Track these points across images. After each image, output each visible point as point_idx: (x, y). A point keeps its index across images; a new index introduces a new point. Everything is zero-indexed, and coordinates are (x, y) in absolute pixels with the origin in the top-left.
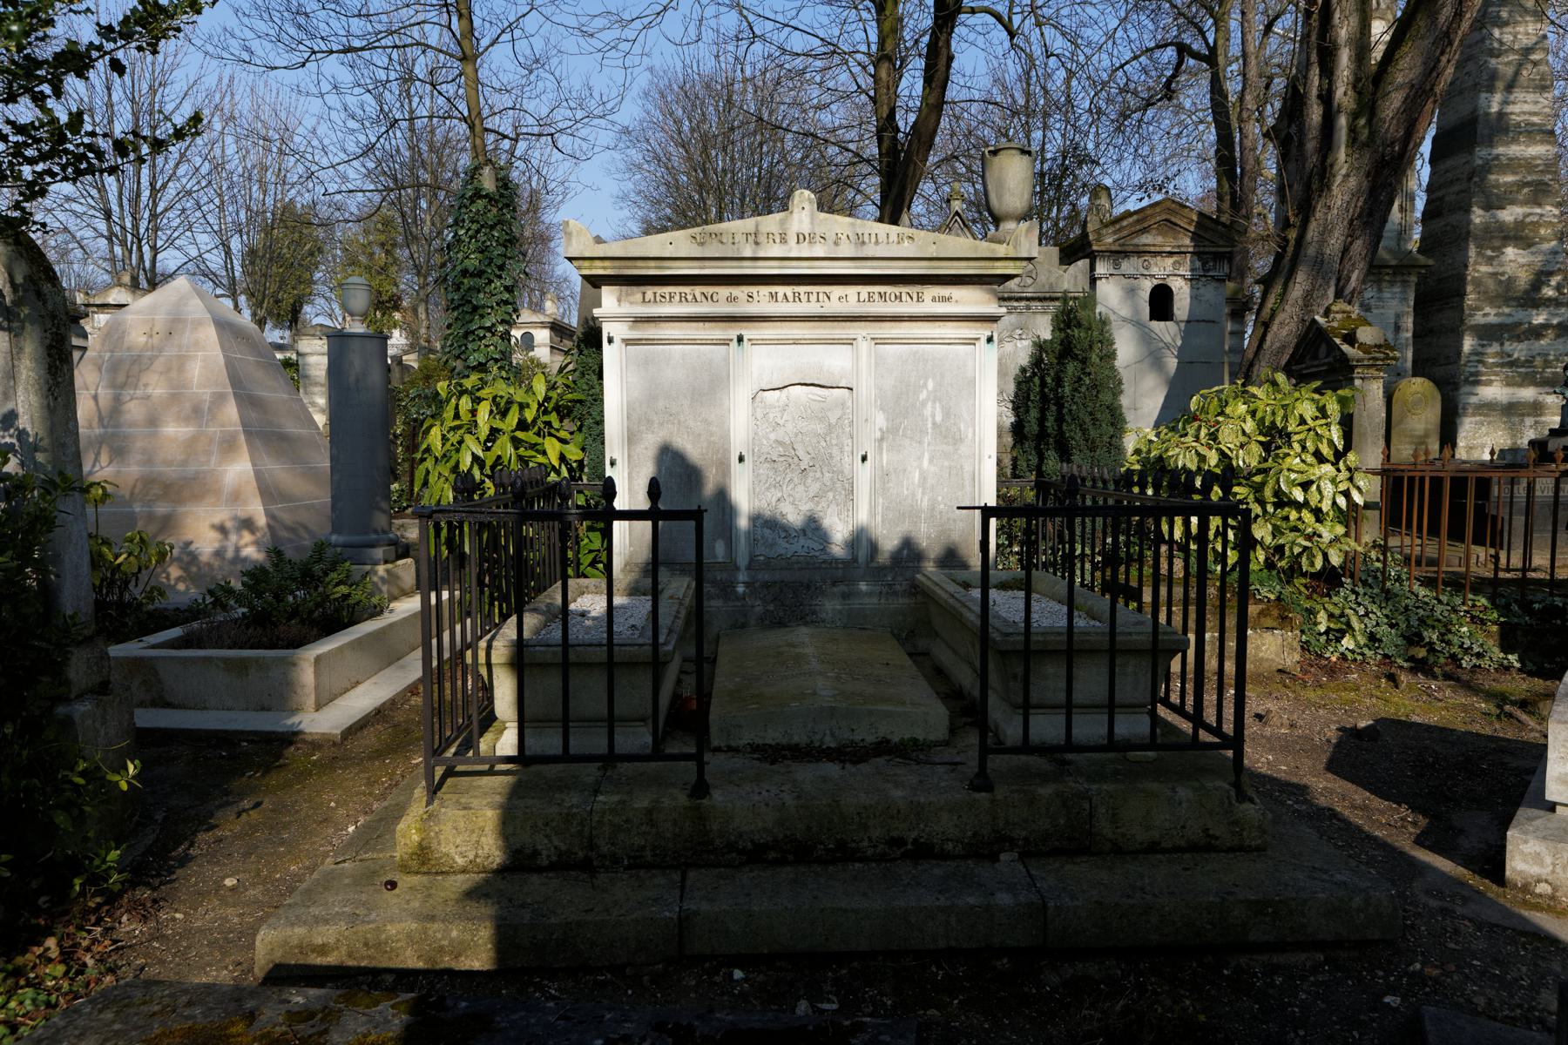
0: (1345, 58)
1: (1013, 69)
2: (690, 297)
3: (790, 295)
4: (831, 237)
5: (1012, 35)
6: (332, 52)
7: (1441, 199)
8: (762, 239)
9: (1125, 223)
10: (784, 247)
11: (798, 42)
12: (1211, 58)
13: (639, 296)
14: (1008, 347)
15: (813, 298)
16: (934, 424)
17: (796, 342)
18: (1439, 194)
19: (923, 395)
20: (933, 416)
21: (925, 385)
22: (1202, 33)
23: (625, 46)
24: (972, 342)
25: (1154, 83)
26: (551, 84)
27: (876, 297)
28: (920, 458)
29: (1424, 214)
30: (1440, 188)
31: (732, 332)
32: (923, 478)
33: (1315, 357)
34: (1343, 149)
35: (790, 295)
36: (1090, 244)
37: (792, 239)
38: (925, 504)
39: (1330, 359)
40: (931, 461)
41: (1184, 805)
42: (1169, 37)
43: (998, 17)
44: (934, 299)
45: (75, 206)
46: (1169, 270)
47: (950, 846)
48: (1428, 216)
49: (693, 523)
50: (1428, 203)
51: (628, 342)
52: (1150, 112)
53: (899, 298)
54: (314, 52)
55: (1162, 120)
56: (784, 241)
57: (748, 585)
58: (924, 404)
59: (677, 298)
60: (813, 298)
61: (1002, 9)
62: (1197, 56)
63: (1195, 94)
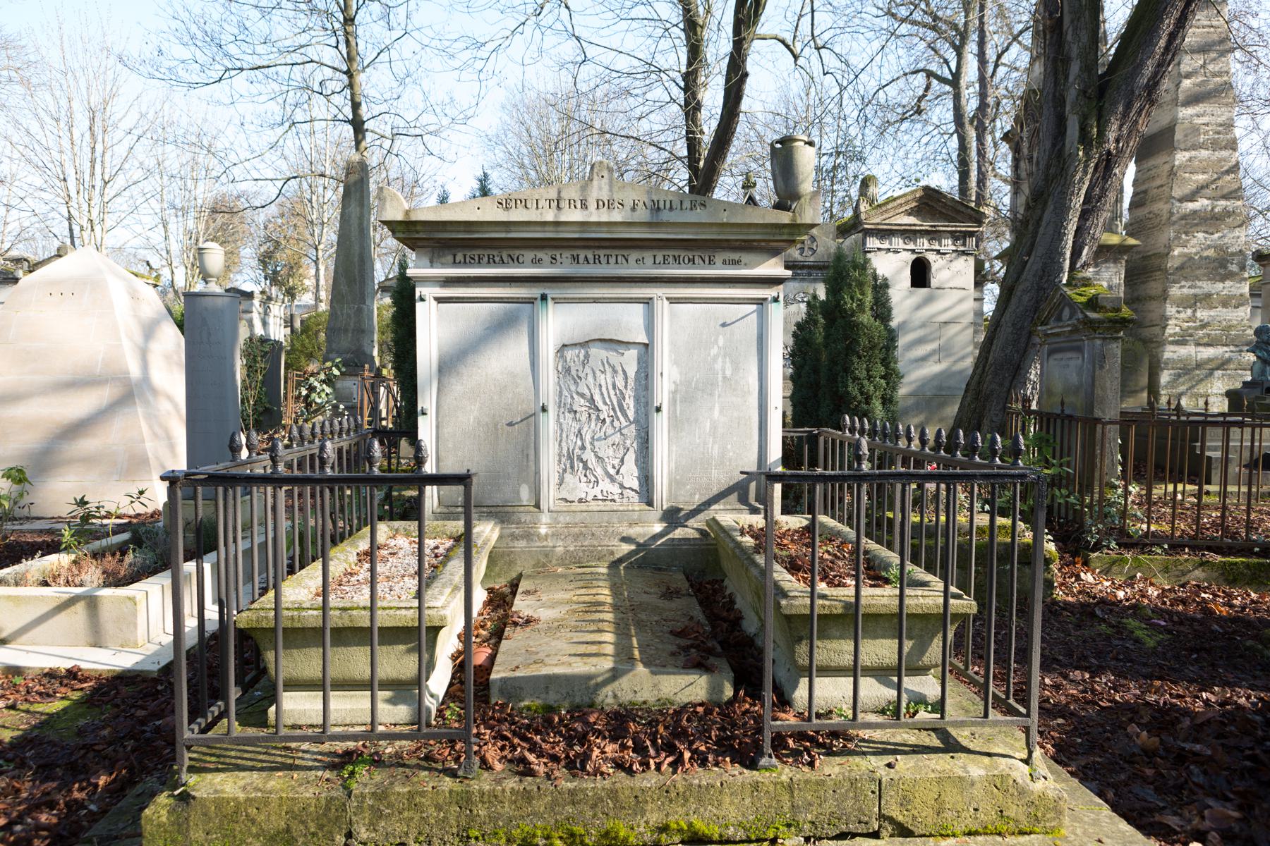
0: (1075, 68)
1: (797, 86)
2: (497, 259)
3: (590, 257)
4: (629, 204)
5: (796, 57)
6: (242, 69)
7: (1145, 192)
8: (564, 204)
9: (889, 206)
10: (585, 212)
11: (623, 63)
12: (955, 81)
13: (450, 258)
14: (793, 308)
15: (612, 260)
16: (724, 377)
17: (596, 301)
18: (1143, 188)
19: (714, 351)
20: (724, 370)
21: (716, 341)
22: (946, 62)
23: (479, 64)
24: (531, 301)
25: (907, 99)
26: (418, 96)
27: (671, 259)
28: (711, 409)
29: (1131, 204)
30: (1144, 182)
31: (535, 292)
32: (714, 428)
33: (1059, 319)
34: (349, 707)
35: (590, 257)
36: (861, 223)
37: (592, 205)
38: (716, 452)
39: (1074, 321)
40: (721, 412)
41: (978, 785)
42: (921, 66)
43: (783, 42)
44: (724, 262)
45: (43, 195)
46: (927, 246)
47: (731, 831)
48: (1133, 206)
49: (461, 488)
50: (1135, 194)
51: (440, 300)
52: (905, 125)
53: (692, 261)
54: (227, 70)
55: (911, 133)
56: (584, 206)
57: (550, 526)
58: (715, 360)
59: (486, 259)
60: (612, 260)
61: (789, 38)
62: (942, 80)
63: (942, 113)
